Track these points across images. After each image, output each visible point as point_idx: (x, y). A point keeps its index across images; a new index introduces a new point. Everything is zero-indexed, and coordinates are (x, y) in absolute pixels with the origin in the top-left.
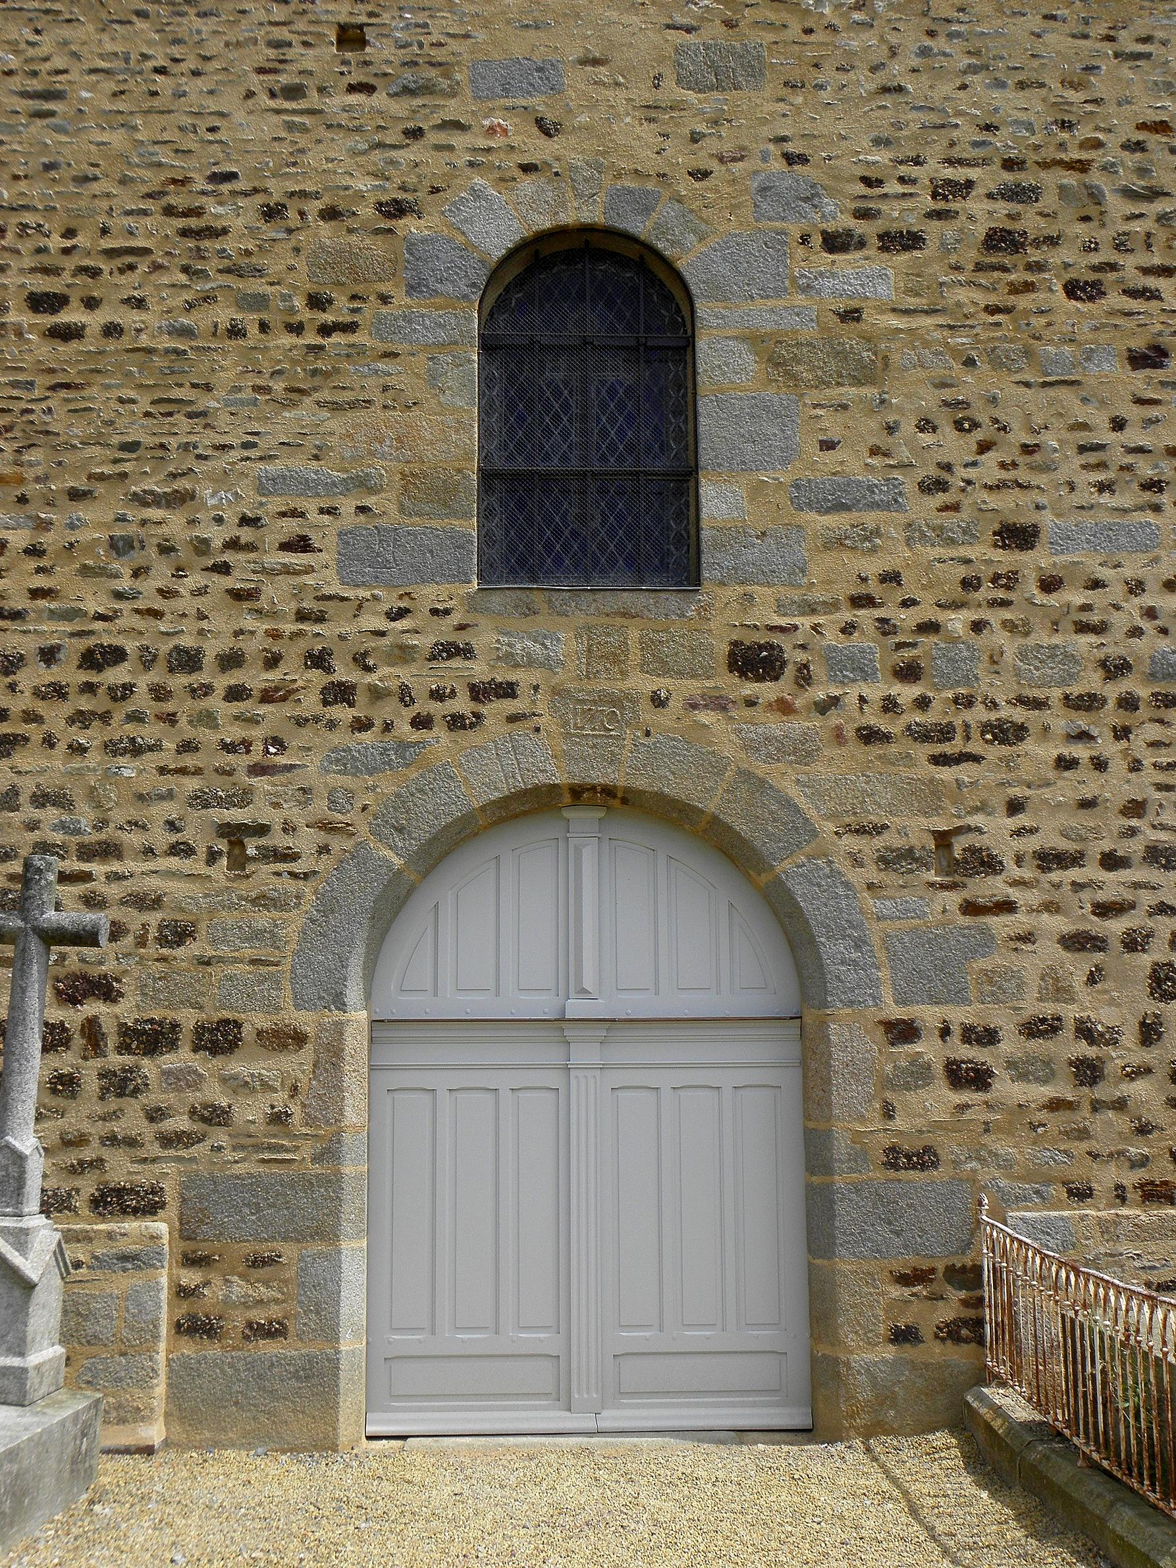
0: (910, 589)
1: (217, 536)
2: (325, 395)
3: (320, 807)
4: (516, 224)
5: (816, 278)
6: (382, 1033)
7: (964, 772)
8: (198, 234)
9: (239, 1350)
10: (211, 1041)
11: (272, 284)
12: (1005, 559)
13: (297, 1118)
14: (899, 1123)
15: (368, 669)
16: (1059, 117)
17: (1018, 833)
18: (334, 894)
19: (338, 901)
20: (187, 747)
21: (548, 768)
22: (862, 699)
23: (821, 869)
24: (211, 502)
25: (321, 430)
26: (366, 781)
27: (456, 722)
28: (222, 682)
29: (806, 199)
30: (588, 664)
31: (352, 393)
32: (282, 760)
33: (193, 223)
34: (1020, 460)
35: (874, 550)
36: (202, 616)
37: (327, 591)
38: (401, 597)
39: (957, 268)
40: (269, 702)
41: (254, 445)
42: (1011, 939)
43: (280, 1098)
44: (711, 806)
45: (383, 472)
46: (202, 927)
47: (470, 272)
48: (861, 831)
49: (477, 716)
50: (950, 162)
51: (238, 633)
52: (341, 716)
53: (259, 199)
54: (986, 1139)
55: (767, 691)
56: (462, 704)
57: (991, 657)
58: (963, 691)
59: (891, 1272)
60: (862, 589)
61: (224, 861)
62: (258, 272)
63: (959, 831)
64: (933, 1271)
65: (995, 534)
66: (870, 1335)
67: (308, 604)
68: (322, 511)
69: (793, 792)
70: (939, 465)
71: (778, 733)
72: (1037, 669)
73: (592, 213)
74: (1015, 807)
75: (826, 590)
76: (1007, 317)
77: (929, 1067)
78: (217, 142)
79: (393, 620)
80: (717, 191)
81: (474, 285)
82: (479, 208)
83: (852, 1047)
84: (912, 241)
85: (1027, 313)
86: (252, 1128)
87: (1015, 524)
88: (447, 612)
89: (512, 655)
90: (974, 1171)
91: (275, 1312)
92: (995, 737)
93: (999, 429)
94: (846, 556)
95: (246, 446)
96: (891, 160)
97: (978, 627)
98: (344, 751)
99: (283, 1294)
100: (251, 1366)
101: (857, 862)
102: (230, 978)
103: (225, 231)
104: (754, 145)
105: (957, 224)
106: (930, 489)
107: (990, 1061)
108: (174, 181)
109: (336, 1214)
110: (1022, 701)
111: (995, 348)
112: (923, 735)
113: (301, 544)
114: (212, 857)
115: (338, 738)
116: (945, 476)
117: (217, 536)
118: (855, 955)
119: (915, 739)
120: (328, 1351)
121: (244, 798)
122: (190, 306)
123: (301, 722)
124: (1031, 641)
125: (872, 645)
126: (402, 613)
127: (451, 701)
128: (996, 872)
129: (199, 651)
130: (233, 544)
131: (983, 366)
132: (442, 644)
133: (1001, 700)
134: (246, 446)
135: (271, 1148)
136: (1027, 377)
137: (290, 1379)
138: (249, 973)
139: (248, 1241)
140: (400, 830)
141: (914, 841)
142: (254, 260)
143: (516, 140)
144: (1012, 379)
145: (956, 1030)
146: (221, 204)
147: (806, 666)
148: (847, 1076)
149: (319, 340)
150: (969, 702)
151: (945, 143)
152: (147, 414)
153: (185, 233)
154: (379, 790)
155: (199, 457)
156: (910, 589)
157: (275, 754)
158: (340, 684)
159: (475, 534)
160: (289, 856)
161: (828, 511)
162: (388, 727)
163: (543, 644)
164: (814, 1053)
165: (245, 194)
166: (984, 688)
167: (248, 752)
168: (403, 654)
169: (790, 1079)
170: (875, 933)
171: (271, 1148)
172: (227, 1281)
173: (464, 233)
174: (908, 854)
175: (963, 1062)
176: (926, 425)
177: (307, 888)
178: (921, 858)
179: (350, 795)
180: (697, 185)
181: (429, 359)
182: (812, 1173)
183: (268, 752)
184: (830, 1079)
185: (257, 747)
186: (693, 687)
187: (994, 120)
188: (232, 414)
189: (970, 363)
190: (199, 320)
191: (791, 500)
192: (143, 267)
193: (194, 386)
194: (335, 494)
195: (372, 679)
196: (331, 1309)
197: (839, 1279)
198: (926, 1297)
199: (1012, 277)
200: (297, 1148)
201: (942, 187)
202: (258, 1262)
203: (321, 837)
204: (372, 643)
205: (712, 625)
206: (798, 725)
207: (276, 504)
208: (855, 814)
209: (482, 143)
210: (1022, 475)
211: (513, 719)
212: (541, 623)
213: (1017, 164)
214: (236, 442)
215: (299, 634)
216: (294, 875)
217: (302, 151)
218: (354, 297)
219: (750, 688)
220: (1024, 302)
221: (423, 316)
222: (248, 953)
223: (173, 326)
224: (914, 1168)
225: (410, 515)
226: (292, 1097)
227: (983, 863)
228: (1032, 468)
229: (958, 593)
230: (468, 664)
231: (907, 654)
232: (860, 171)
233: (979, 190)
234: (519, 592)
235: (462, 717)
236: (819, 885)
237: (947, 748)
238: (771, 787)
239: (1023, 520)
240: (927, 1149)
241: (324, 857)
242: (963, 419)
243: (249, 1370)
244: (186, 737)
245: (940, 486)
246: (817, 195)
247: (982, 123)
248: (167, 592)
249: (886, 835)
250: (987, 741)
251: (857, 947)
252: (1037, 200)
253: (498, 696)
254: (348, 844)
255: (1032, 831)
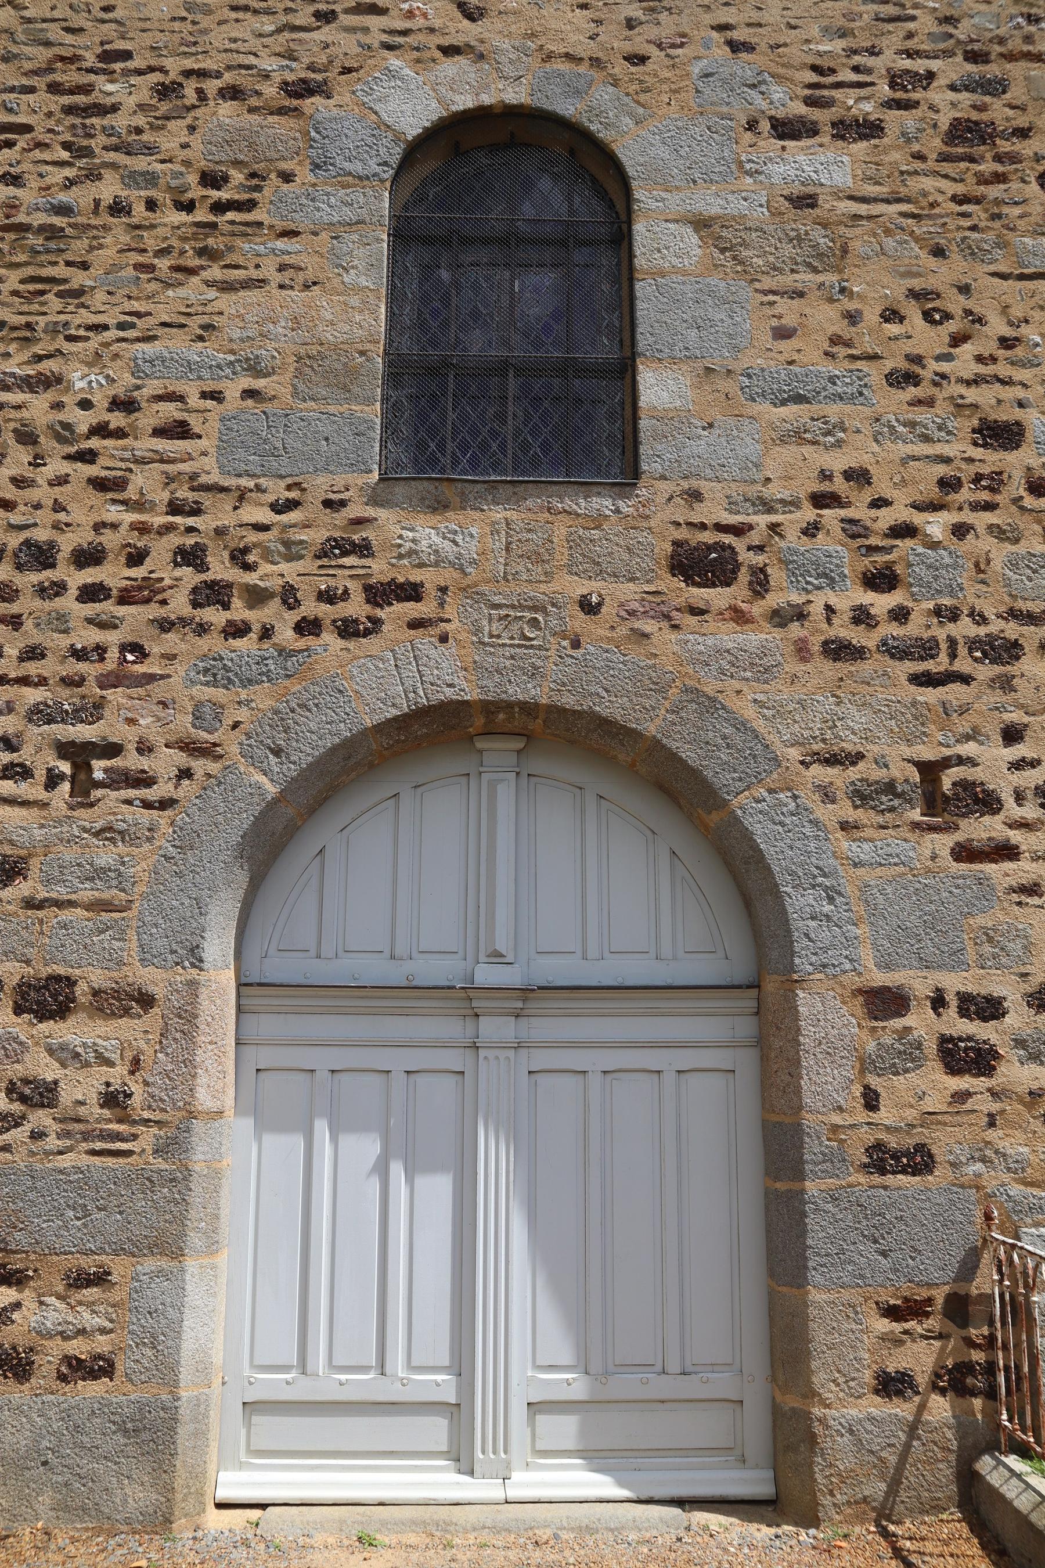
0: (882, 487)
1: (83, 421)
2: (215, 272)
3: (183, 723)
4: (434, 104)
5: (765, 164)
6: (255, 999)
7: (953, 692)
8: (87, 111)
9: (52, 1393)
10: (38, 1003)
11: (163, 161)
12: (992, 459)
13: (136, 1101)
14: (885, 1115)
15: (248, 567)
16: (1025, 10)
17: (1018, 765)
18: (195, 827)
19: (198, 836)
20: (33, 653)
21: (456, 681)
22: (829, 609)
23: (786, 805)
24: (80, 385)
25: (209, 309)
26: (238, 694)
27: (348, 629)
28: (78, 578)
29: (753, 86)
30: (506, 565)
31: (244, 272)
32: (140, 669)
33: (81, 99)
34: (1001, 353)
35: (839, 444)
36: (58, 507)
37: (204, 479)
38: (289, 488)
39: (920, 157)
40: (130, 604)
41: (133, 326)
42: (1014, 892)
43: (118, 1074)
44: (651, 728)
45: (276, 354)
46: (35, 863)
47: (383, 151)
48: (832, 760)
49: (377, 622)
50: (910, 54)
51: (98, 527)
52: (213, 619)
53: (156, 77)
54: (992, 1135)
55: (717, 597)
56: (356, 607)
57: (977, 565)
58: (947, 601)
59: (877, 1303)
60: (826, 487)
61: (66, 786)
62: (150, 149)
63: (946, 763)
64: (929, 1301)
65: (974, 431)
66: (852, 1384)
67: (184, 493)
68: (204, 395)
69: (749, 712)
70: (908, 357)
71: (730, 645)
72: (1030, 579)
73: (515, 95)
74: (1012, 735)
75: (785, 487)
76: (977, 207)
77: (919, 1046)
78: (110, 21)
79: (279, 512)
80: (656, 75)
81: (385, 164)
82: (393, 88)
83: (826, 1020)
84: (870, 129)
85: (997, 202)
86: (82, 1111)
87: (996, 421)
88: (343, 503)
89: (416, 552)
90: (979, 1176)
91: (102, 1344)
92: (985, 654)
93: (973, 322)
94: (807, 450)
95: (121, 326)
96: (843, 50)
97: (960, 531)
98: (214, 659)
99: (111, 1321)
100: (66, 1415)
101: (827, 796)
102: (64, 926)
103: (114, 108)
104: (696, 32)
105: (917, 113)
106: (899, 383)
107: (994, 1038)
108: (62, 59)
109: (181, 1220)
110: (1013, 614)
111: (965, 238)
112: (898, 652)
113: (180, 430)
114: (53, 780)
115: (212, 643)
116: (918, 370)
117: (83, 421)
118: (827, 908)
119: (893, 656)
120: (164, 1397)
121: (94, 711)
122: (70, 183)
123: (165, 625)
124: (1021, 549)
125: (839, 548)
126: (292, 505)
127: (342, 604)
128: (996, 812)
129: (52, 545)
130: (101, 430)
131: (955, 256)
132: (335, 540)
133: (990, 613)
134: (121, 326)
135: (104, 1136)
136: (1003, 268)
137: (114, 1433)
138: (88, 920)
139: (72, 1253)
140: (277, 752)
141: (895, 773)
142: (145, 137)
143: (437, 23)
144: (986, 270)
145: (952, 999)
146: (112, 81)
147: (762, 570)
148: (820, 1056)
149: (212, 218)
150: (954, 616)
151: (902, 34)
152: (15, 293)
153: (69, 110)
154: (253, 705)
155: (70, 338)
156: (882, 487)
157: (134, 662)
158: (215, 583)
159: (378, 421)
160: (145, 780)
161: (784, 403)
162: (266, 633)
163: (454, 542)
164: (778, 1028)
165: (140, 72)
166: (971, 600)
167: (102, 659)
168: (291, 551)
169: (746, 1062)
170: (848, 881)
171: (104, 1136)
172: (41, 1303)
173: (376, 113)
174: (889, 787)
175: (961, 1039)
176: (892, 315)
177: (162, 818)
178: (903, 793)
179: (218, 707)
180: (633, 69)
181: (332, 238)
182: (777, 1179)
183: (125, 660)
184: (799, 1061)
185: (113, 654)
186: (629, 591)
187: (955, 13)
188: (109, 293)
189: (938, 252)
190: (81, 197)
191: (742, 389)
192: (21, 144)
193: (68, 264)
194: (220, 378)
195: (251, 578)
196: (170, 1343)
197: (812, 1312)
198: (922, 1336)
199: (982, 168)
200: (135, 1137)
201: (900, 77)
202: (81, 1280)
203: (181, 758)
204: (253, 537)
205: (652, 524)
206: (753, 638)
207: (153, 387)
208: (824, 740)
209: (400, 25)
210: (1003, 370)
211: (416, 624)
212: (452, 520)
213: (981, 56)
214: (112, 322)
215: (169, 528)
216: (147, 805)
217: (205, 32)
218: (253, 175)
219: (699, 595)
220: (994, 191)
221: (328, 194)
222: (86, 894)
223: (51, 204)
224: (904, 1172)
225: (305, 401)
226: (132, 1073)
227: (977, 801)
228: (1012, 364)
229: (934, 492)
230: (364, 562)
231: (881, 558)
232: (810, 60)
233: (941, 81)
234: (426, 483)
235: (356, 621)
236: (782, 824)
237: (929, 666)
238: (724, 708)
239: (1004, 416)
240: (921, 1148)
241: (186, 782)
242: (935, 309)
243: (63, 1419)
244: (31, 642)
245: (910, 379)
246: (764, 82)
247: (940, 15)
248: (22, 482)
249: (861, 765)
250: (976, 660)
251: (831, 900)
252: (1004, 92)
253: (400, 600)
254: (213, 767)
255: (1034, 763)
